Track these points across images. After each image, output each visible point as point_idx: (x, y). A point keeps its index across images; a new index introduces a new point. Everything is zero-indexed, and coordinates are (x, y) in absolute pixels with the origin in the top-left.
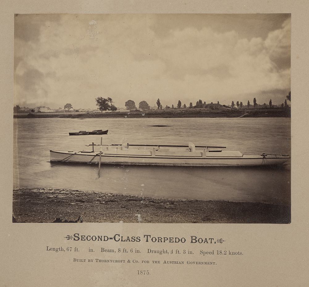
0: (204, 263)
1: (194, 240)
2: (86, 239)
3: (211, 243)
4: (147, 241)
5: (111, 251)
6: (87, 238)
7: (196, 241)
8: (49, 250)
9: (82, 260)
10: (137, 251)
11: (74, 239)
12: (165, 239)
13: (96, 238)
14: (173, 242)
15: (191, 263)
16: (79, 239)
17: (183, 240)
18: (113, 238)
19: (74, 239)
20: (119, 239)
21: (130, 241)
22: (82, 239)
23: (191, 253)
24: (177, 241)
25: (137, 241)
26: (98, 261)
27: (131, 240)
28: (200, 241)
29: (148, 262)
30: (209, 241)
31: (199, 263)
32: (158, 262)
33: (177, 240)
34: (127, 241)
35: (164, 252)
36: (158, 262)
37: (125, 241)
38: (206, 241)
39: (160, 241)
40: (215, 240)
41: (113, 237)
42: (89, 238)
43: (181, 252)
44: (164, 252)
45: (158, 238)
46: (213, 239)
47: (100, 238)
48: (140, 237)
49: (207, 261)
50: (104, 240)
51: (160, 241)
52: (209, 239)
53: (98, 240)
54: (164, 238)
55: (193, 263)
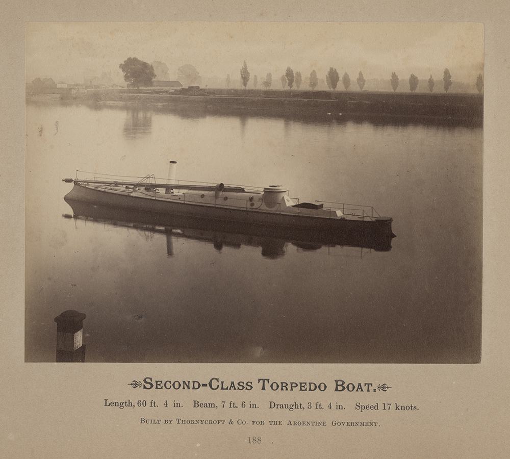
0: (360, 424)
1: (340, 386)
2: (164, 387)
3: (368, 390)
4: (263, 388)
5: (211, 406)
6: (165, 385)
7: (344, 388)
8: (109, 405)
9: (154, 420)
10: (176, 404)
11: (145, 387)
12: (293, 385)
13: (180, 385)
14: (306, 390)
15: (339, 424)
16: (152, 386)
17: (322, 387)
18: (208, 385)
19: (145, 387)
20: (218, 386)
21: (235, 389)
22: (157, 386)
23: (340, 407)
24: (313, 388)
25: (247, 389)
26: (180, 422)
27: (237, 388)
28: (351, 387)
29: (262, 423)
30: (365, 388)
31: (352, 424)
32: (278, 424)
33: (313, 387)
34: (230, 389)
35: (297, 407)
36: (278, 424)
37: (227, 389)
38: (360, 387)
39: (284, 388)
40: (375, 386)
41: (208, 383)
42: (168, 385)
43: (325, 405)
44: (297, 407)
45: (282, 383)
46: (372, 384)
47: (186, 385)
48: (251, 383)
49: (365, 421)
50: (194, 388)
51: (284, 388)
52: (365, 384)
53: (184, 388)
54: (300, 383)
55: (342, 424)
